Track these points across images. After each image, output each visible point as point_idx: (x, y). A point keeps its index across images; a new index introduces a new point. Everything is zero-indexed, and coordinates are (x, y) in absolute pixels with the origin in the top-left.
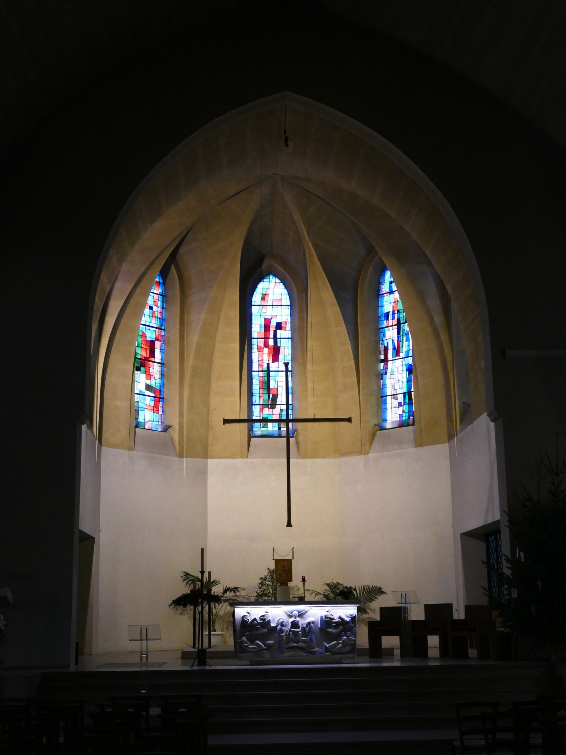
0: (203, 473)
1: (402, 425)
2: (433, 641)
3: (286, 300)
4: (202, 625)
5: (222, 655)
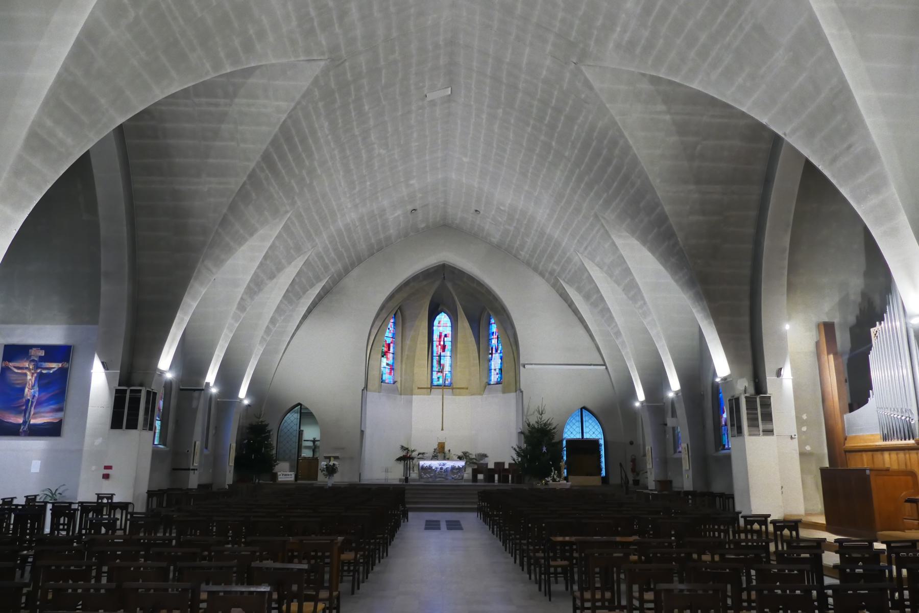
0: (411, 402)
1: (498, 383)
2: (496, 476)
3: (449, 324)
4: (407, 469)
5: (414, 480)
